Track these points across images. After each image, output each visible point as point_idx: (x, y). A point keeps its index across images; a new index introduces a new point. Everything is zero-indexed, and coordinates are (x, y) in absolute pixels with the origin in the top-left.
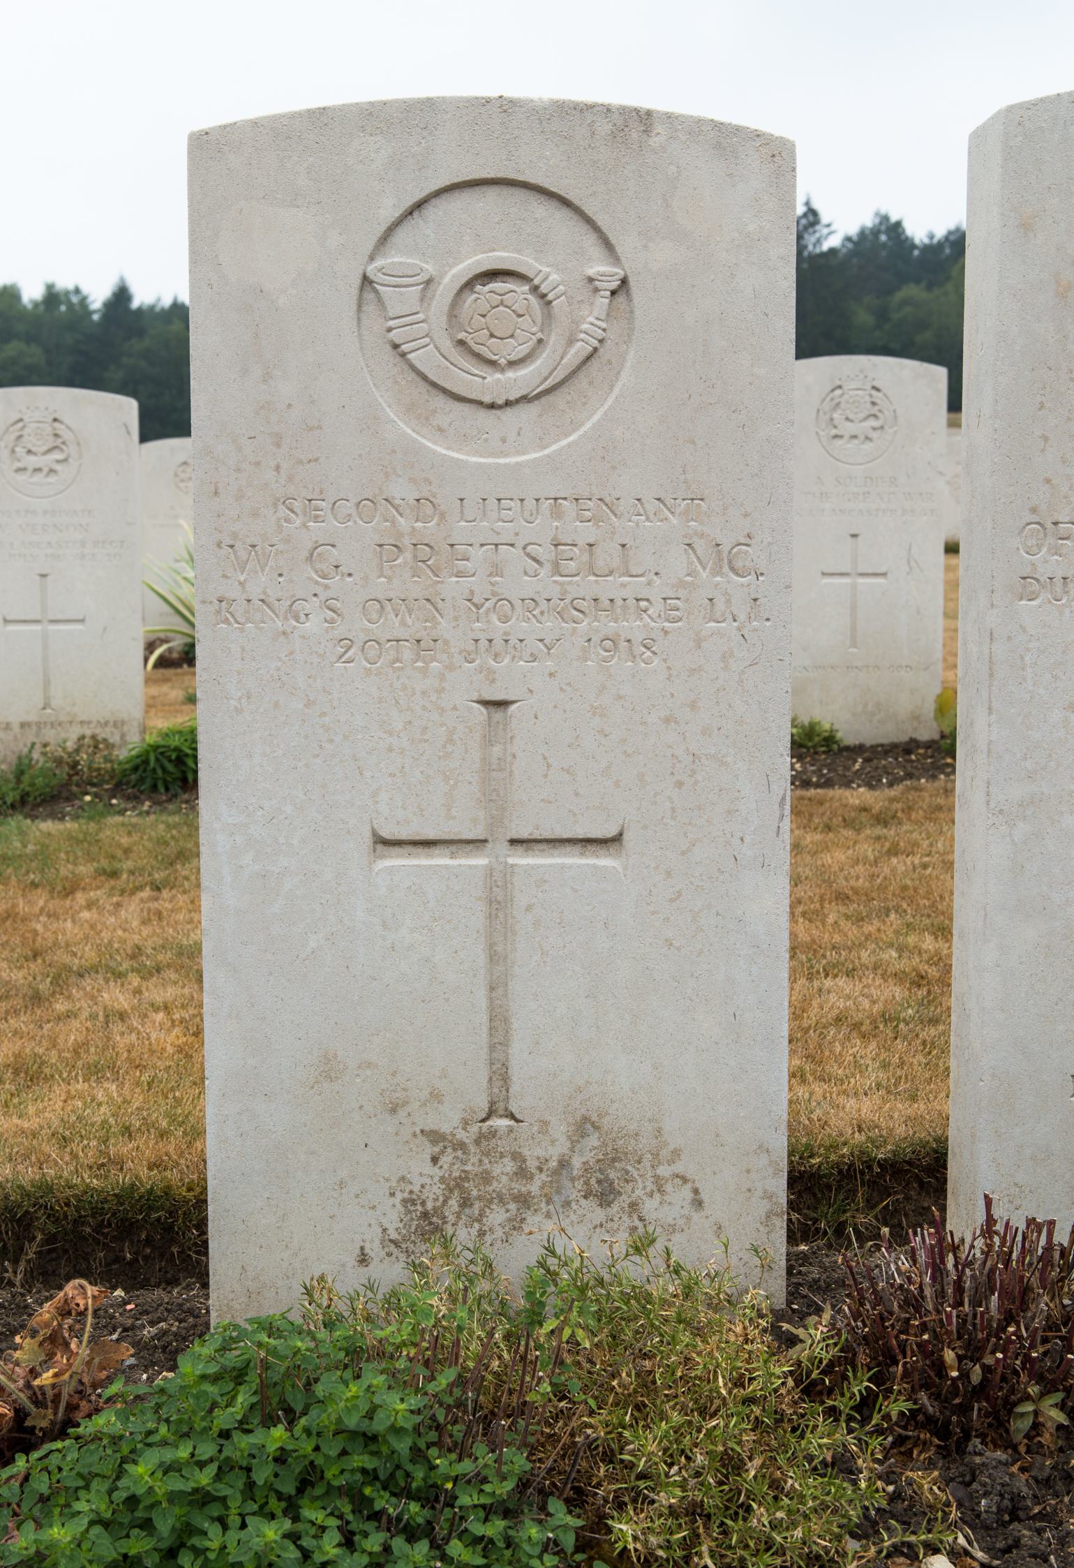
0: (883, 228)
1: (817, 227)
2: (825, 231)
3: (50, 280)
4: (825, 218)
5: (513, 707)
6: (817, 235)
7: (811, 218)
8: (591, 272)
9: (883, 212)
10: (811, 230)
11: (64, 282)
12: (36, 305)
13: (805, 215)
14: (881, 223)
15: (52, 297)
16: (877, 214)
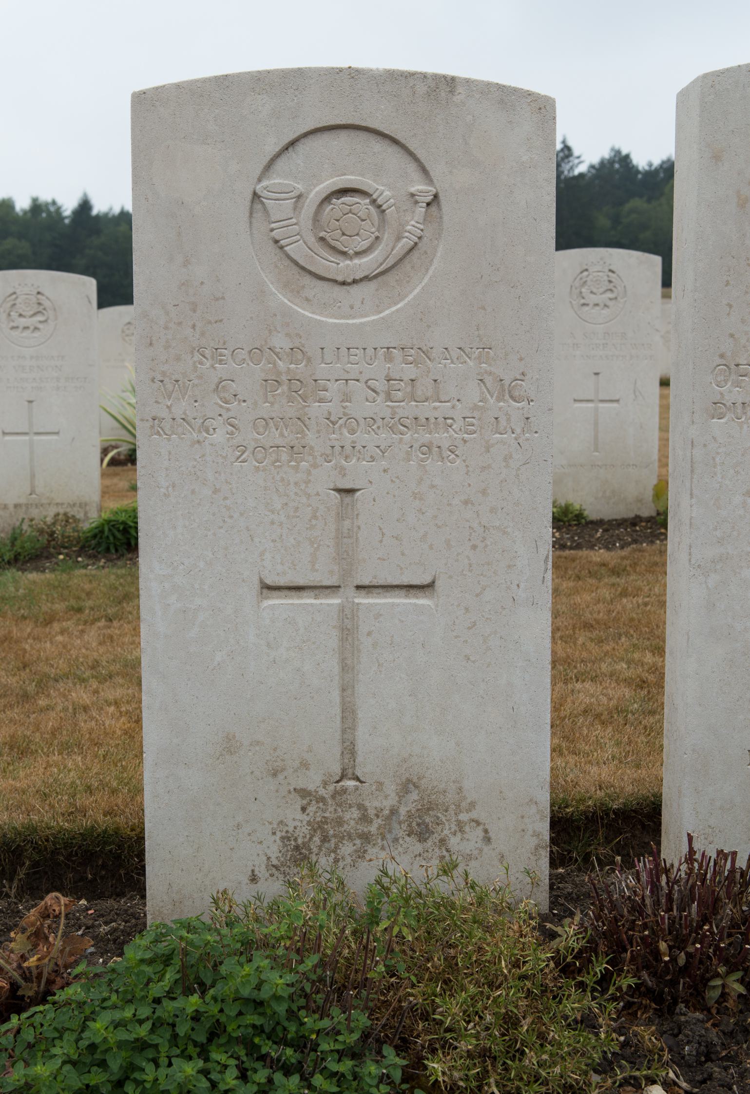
0: (617, 159)
1: (571, 159)
2: (576, 161)
3: (35, 195)
4: (576, 152)
5: (358, 493)
6: (571, 164)
7: (566, 152)
8: (413, 190)
9: (617, 147)
10: (566, 161)
11: (45, 197)
12: (25, 212)
13: (562, 150)
14: (615, 156)
15: (37, 207)
16: (613, 149)
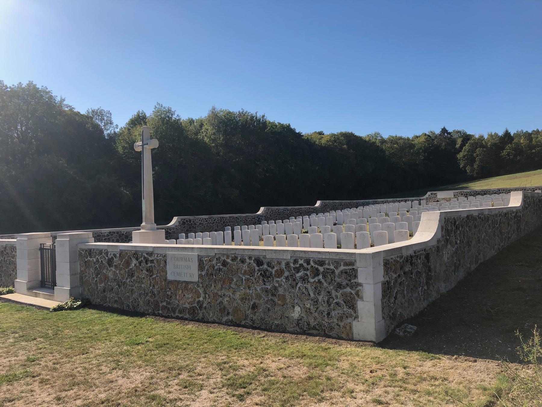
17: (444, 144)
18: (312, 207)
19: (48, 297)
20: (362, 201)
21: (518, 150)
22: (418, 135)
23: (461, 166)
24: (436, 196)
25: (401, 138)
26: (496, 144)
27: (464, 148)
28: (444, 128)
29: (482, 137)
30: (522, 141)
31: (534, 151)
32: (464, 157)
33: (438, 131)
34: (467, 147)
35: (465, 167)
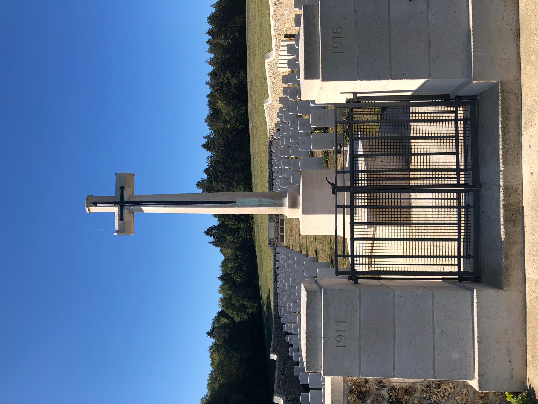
15: (221, 292)
17: (223, 335)
18: (277, 363)
19: (512, 123)
20: (273, 323)
21: (238, 269)
22: (211, 362)
23: (247, 318)
24: (272, 239)
25: (211, 375)
26: (229, 287)
27: (230, 315)
28: (208, 333)
29: (221, 299)
30: (230, 266)
31: (240, 257)
32: (238, 314)
33: (211, 341)
34: (229, 312)
35: (248, 314)
